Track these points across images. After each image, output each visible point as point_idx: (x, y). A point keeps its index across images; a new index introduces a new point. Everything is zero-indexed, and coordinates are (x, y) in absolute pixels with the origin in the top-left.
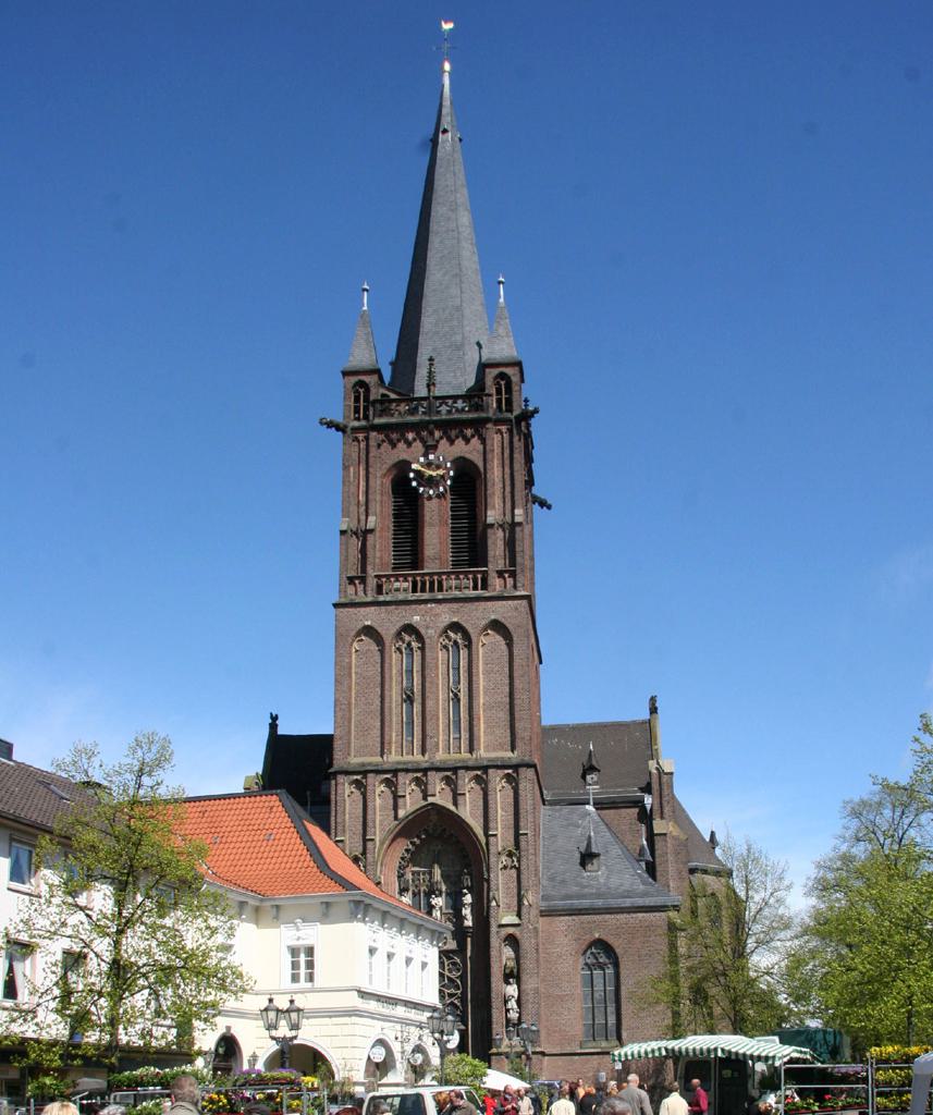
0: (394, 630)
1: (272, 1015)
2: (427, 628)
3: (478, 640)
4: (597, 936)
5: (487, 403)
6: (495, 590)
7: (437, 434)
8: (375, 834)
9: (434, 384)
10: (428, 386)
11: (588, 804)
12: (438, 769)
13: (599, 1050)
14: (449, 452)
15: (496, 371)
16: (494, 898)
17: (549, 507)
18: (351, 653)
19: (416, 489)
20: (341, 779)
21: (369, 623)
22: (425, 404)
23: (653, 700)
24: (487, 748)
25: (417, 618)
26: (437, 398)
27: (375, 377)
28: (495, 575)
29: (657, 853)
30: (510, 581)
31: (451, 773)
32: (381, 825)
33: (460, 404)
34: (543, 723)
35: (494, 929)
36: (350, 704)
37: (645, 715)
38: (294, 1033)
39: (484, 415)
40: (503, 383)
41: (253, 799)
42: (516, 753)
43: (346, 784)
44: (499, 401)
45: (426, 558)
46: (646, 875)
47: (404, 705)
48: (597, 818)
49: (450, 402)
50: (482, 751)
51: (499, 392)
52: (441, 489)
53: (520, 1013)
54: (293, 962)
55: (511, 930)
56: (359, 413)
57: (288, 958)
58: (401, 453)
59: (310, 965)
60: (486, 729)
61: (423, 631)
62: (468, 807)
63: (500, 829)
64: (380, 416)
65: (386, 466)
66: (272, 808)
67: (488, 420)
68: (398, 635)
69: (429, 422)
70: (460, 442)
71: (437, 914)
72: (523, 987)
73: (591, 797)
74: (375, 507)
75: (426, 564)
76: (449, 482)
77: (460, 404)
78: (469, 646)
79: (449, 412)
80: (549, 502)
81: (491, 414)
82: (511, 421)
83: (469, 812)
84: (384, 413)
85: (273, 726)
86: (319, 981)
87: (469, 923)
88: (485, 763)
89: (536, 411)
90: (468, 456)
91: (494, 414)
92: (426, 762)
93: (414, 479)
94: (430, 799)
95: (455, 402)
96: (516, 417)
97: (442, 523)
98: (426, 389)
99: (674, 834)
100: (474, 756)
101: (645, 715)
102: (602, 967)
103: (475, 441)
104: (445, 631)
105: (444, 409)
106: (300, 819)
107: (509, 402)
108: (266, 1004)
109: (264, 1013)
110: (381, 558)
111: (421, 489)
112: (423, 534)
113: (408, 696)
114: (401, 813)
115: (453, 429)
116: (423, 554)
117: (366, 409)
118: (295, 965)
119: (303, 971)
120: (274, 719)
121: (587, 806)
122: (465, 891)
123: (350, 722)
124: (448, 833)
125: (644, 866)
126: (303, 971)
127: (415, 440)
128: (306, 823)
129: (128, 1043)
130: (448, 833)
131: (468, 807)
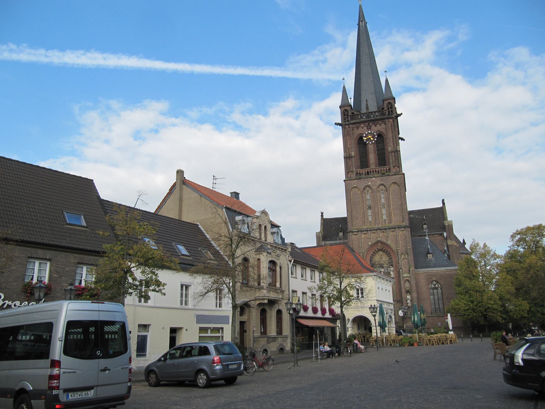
0: (363, 187)
2: (373, 186)
7: (371, 124)
8: (362, 250)
10: (366, 109)
13: (437, 316)
14: (376, 129)
15: (387, 102)
17: (404, 140)
22: (366, 115)
23: (443, 201)
25: (370, 183)
26: (370, 113)
27: (350, 107)
29: (450, 251)
33: (377, 114)
34: (408, 210)
35: (401, 278)
37: (441, 205)
39: (385, 117)
40: (390, 105)
41: (337, 246)
44: (389, 111)
46: (448, 259)
49: (374, 113)
50: (393, 223)
55: (407, 278)
58: (360, 131)
59: (362, 293)
61: (372, 187)
64: (352, 120)
65: (355, 136)
70: (378, 126)
75: (371, 166)
77: (377, 114)
79: (374, 117)
81: (387, 116)
85: (322, 216)
94: (379, 239)
97: (375, 152)
99: (455, 245)
101: (441, 205)
102: (437, 288)
103: (383, 125)
104: (379, 186)
105: (372, 116)
115: (375, 121)
116: (369, 162)
120: (322, 213)
121: (426, 238)
124: (386, 250)
126: (360, 295)
127: (364, 126)
130: (386, 250)
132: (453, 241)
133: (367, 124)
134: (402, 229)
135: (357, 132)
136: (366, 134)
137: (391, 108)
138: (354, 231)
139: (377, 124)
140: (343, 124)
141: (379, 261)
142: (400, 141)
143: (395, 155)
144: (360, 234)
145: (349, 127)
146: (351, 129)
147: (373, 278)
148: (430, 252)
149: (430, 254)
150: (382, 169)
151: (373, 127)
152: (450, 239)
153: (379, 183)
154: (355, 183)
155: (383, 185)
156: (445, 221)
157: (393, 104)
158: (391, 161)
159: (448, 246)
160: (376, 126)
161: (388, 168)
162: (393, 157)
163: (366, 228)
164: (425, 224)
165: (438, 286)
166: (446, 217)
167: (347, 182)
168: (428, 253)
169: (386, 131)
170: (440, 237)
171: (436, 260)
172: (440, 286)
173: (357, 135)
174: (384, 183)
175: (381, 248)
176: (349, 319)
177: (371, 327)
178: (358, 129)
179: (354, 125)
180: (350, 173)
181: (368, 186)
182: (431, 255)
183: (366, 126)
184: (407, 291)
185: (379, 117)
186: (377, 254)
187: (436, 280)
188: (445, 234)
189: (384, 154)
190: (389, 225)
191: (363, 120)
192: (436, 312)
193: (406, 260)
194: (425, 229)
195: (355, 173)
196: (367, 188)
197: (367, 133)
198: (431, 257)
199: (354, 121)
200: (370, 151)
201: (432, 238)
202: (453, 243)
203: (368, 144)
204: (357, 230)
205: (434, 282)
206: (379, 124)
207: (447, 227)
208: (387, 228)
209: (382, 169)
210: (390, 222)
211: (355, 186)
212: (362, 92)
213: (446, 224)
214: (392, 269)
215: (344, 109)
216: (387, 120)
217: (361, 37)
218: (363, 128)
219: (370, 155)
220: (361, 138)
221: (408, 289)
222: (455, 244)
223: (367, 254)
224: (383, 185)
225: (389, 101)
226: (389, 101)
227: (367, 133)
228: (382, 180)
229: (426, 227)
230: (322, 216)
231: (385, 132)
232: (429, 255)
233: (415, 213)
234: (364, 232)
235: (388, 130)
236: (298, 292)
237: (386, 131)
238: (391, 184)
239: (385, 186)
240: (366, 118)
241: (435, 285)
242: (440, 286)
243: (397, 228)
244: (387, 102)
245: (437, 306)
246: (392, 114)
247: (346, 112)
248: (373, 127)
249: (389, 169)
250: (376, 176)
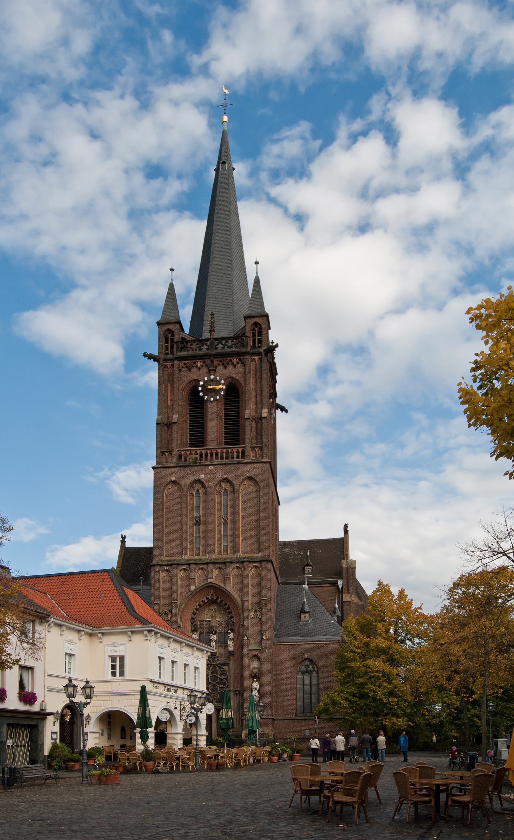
0: (188, 483)
2: (209, 481)
3: (239, 488)
4: (306, 656)
5: (247, 342)
7: (216, 363)
8: (177, 600)
9: (214, 331)
10: (210, 331)
11: (304, 584)
12: (214, 563)
15: (253, 321)
16: (246, 635)
17: (286, 411)
18: (163, 497)
19: (202, 398)
20: (157, 569)
23: (346, 526)
25: (202, 476)
26: (216, 339)
28: (250, 449)
30: (259, 453)
31: (221, 564)
32: (180, 595)
33: (230, 343)
35: (245, 652)
36: (162, 526)
37: (341, 535)
38: (88, 700)
39: (244, 350)
40: (256, 329)
42: (260, 554)
43: (161, 572)
44: (254, 341)
45: (208, 440)
47: (195, 527)
48: (309, 592)
50: (241, 553)
51: (254, 335)
52: (218, 397)
53: (260, 698)
54: (112, 665)
55: (255, 653)
56: (167, 350)
57: (109, 663)
58: (194, 374)
59: (122, 666)
60: (242, 540)
61: (206, 484)
62: (232, 584)
63: (250, 597)
64: (181, 351)
65: (184, 384)
66: (104, 579)
67: (247, 353)
68: (192, 485)
69: (210, 355)
70: (230, 367)
71: (214, 644)
72: (262, 683)
73: (306, 581)
74: (177, 408)
76: (222, 393)
77: (230, 343)
78: (233, 492)
79: (223, 348)
80: (286, 408)
81: (249, 349)
82: (261, 353)
83: (230, 588)
84: (182, 349)
85: (123, 542)
86: (128, 675)
87: (231, 648)
88: (242, 560)
89: (277, 346)
90: (235, 376)
91: (251, 350)
92: (207, 559)
93: (201, 391)
94: (210, 580)
95: (227, 342)
96: (265, 351)
99: (355, 601)
100: (236, 556)
101: (341, 535)
102: (310, 672)
103: (239, 367)
104: (219, 483)
105: (220, 346)
106: (121, 585)
107: (260, 341)
108: (67, 682)
109: (66, 688)
110: (181, 440)
111: (206, 397)
112: (207, 425)
113: (197, 521)
114: (193, 588)
116: (206, 437)
117: (172, 347)
118: (113, 667)
119: (118, 670)
121: (304, 586)
122: (229, 631)
123: (163, 537)
125: (336, 619)
127: (202, 366)
128: (124, 588)
131: (232, 584)
132: (353, 596)
133: (208, 362)
134: (256, 564)
135: (188, 376)
136: (205, 382)
137: (260, 334)
138: (164, 563)
139: (228, 364)
140: (160, 358)
141: (210, 621)
142: (278, 411)
143: (257, 427)
144: (175, 570)
145: (173, 366)
146: (176, 369)
147: (146, 636)
148: (306, 609)
149: (305, 612)
150: (230, 450)
151: (220, 368)
152: (348, 592)
153: (220, 476)
154: (173, 475)
155: (226, 480)
156: (342, 561)
157: (263, 326)
158: (248, 436)
159: (342, 604)
160: (225, 367)
161: (240, 450)
162: (254, 430)
163: (188, 560)
164: (308, 565)
165: (312, 669)
166: (347, 555)
167: (158, 470)
168: (303, 611)
169: (245, 379)
170: (332, 588)
171: (314, 624)
172: (316, 669)
173: (187, 381)
174: (230, 478)
175: (215, 598)
176: (89, 717)
177: (166, 735)
178: (190, 370)
179: (184, 362)
180: (167, 454)
181: (199, 481)
182: (307, 615)
183: (206, 366)
184: (253, 675)
185: (234, 349)
186: (207, 609)
187: (310, 657)
188: (340, 583)
189: (237, 423)
190: (232, 556)
191: (201, 352)
192: (304, 713)
193: (257, 620)
194: (308, 574)
195: (175, 454)
196: (197, 486)
197: (206, 379)
198: (307, 619)
199: (184, 353)
200: (209, 416)
201: (316, 589)
202: (353, 598)
203: (207, 400)
204: (169, 563)
205: (307, 663)
206: (232, 364)
207: (344, 571)
208: (228, 560)
209: (230, 450)
210: (235, 550)
211: (173, 479)
212: (207, 302)
213: (344, 566)
214: (231, 636)
215: (165, 327)
216: (248, 357)
217: (218, 194)
218: (199, 369)
219: (209, 422)
220: (194, 391)
221: (255, 671)
222: (355, 599)
223: (185, 607)
224: (226, 480)
225: (257, 320)
226: (257, 320)
227: (206, 379)
228: (227, 471)
229: (310, 571)
230: (123, 542)
231: (242, 381)
232: (303, 616)
233: (293, 545)
234: (183, 567)
235: (248, 376)
236: (35, 670)
237: (245, 379)
238: (243, 480)
239: (231, 484)
240: (208, 349)
241: (307, 666)
242: (316, 669)
243: (247, 561)
244: (253, 321)
245: (307, 702)
246: (259, 347)
247: (169, 336)
248: (220, 368)
249: (243, 453)
250: (216, 463)
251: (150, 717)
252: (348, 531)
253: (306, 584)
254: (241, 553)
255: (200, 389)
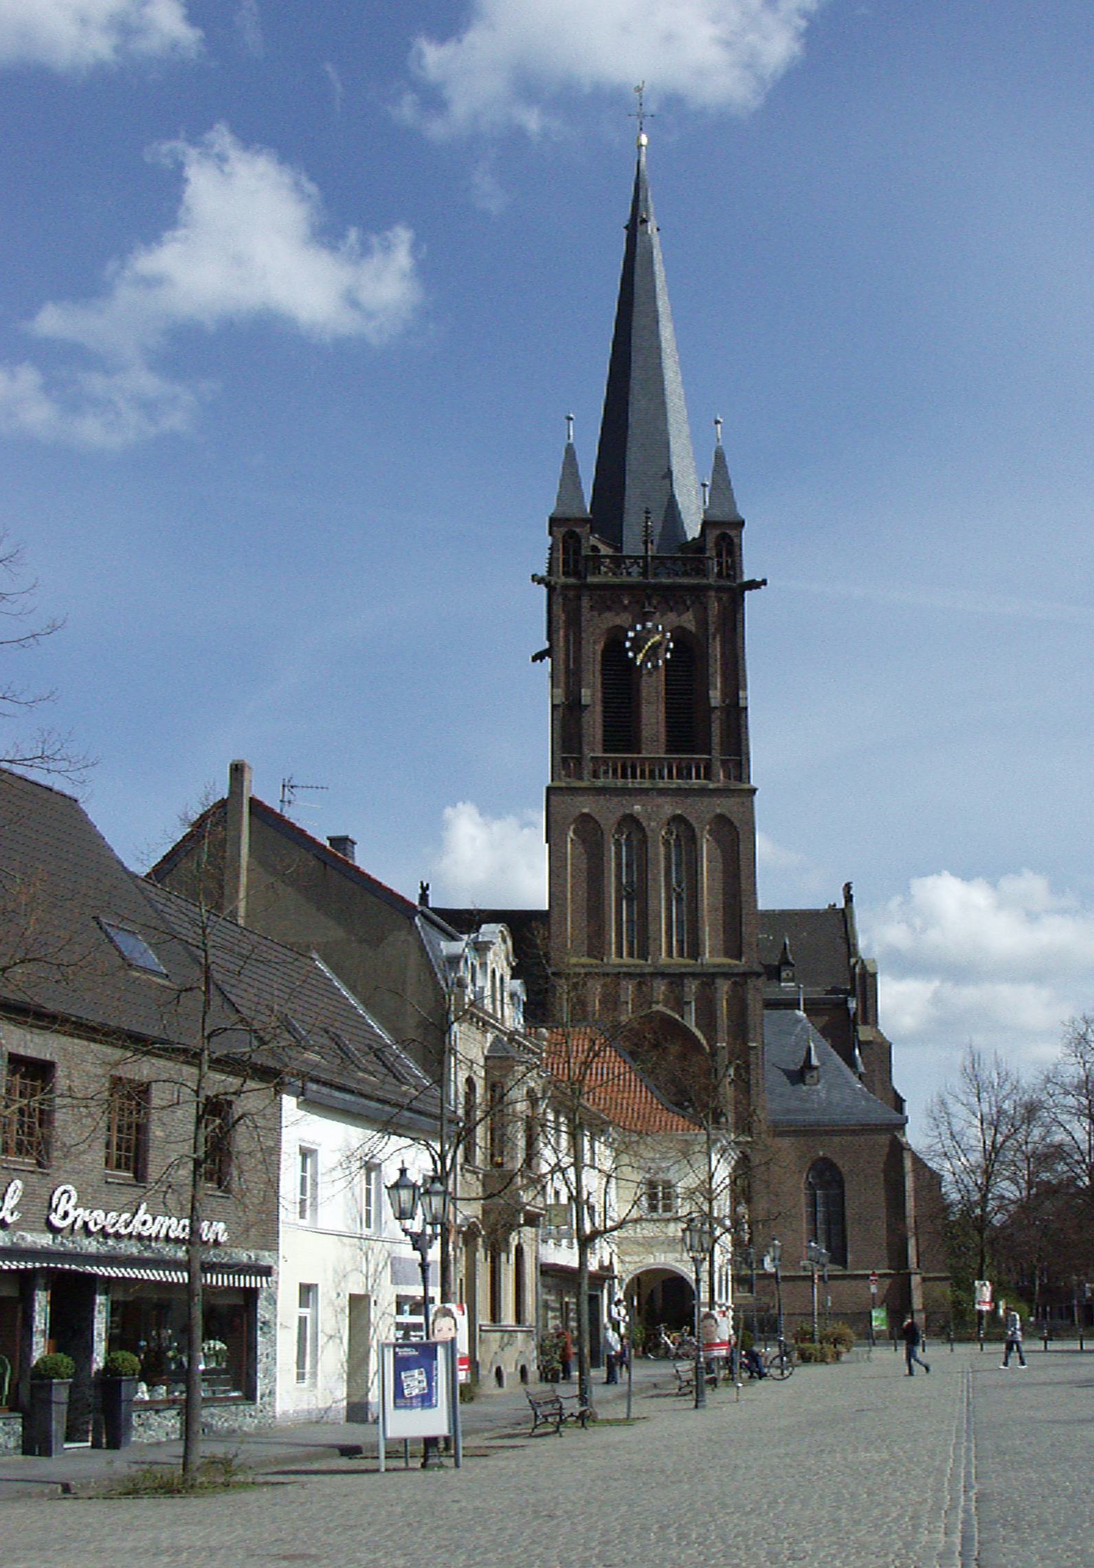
1: (405, 1195)
2: (650, 819)
6: (719, 781)
11: (799, 1009)
18: (566, 841)
21: (586, 810)
23: (848, 887)
24: (711, 956)
25: (637, 808)
31: (676, 979)
39: (705, 581)
45: (644, 740)
50: (707, 955)
67: (708, 587)
88: (712, 970)
92: (649, 966)
93: (630, 649)
98: (643, 547)
100: (699, 961)
101: (841, 904)
121: (797, 1011)
129: (159, 1299)
210: (695, 952)
251: (486, 1250)
252: (851, 896)
253: (802, 1007)
254: (707, 955)
255: (628, 644)
